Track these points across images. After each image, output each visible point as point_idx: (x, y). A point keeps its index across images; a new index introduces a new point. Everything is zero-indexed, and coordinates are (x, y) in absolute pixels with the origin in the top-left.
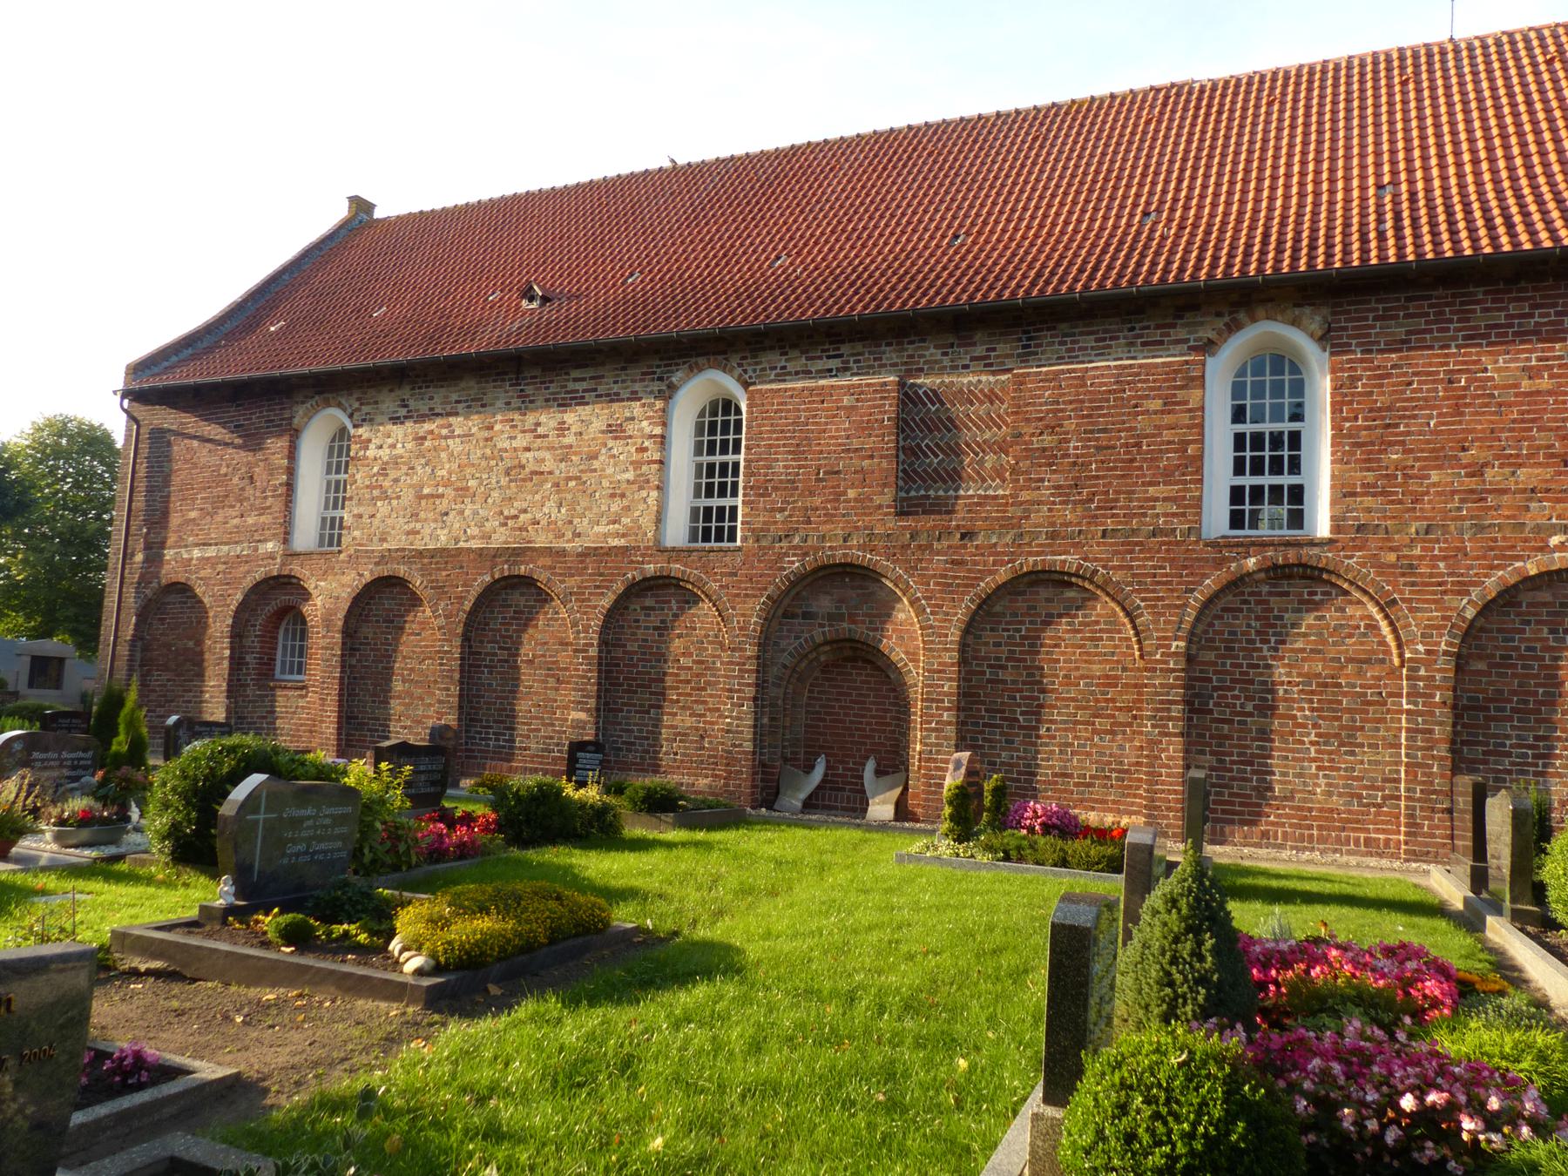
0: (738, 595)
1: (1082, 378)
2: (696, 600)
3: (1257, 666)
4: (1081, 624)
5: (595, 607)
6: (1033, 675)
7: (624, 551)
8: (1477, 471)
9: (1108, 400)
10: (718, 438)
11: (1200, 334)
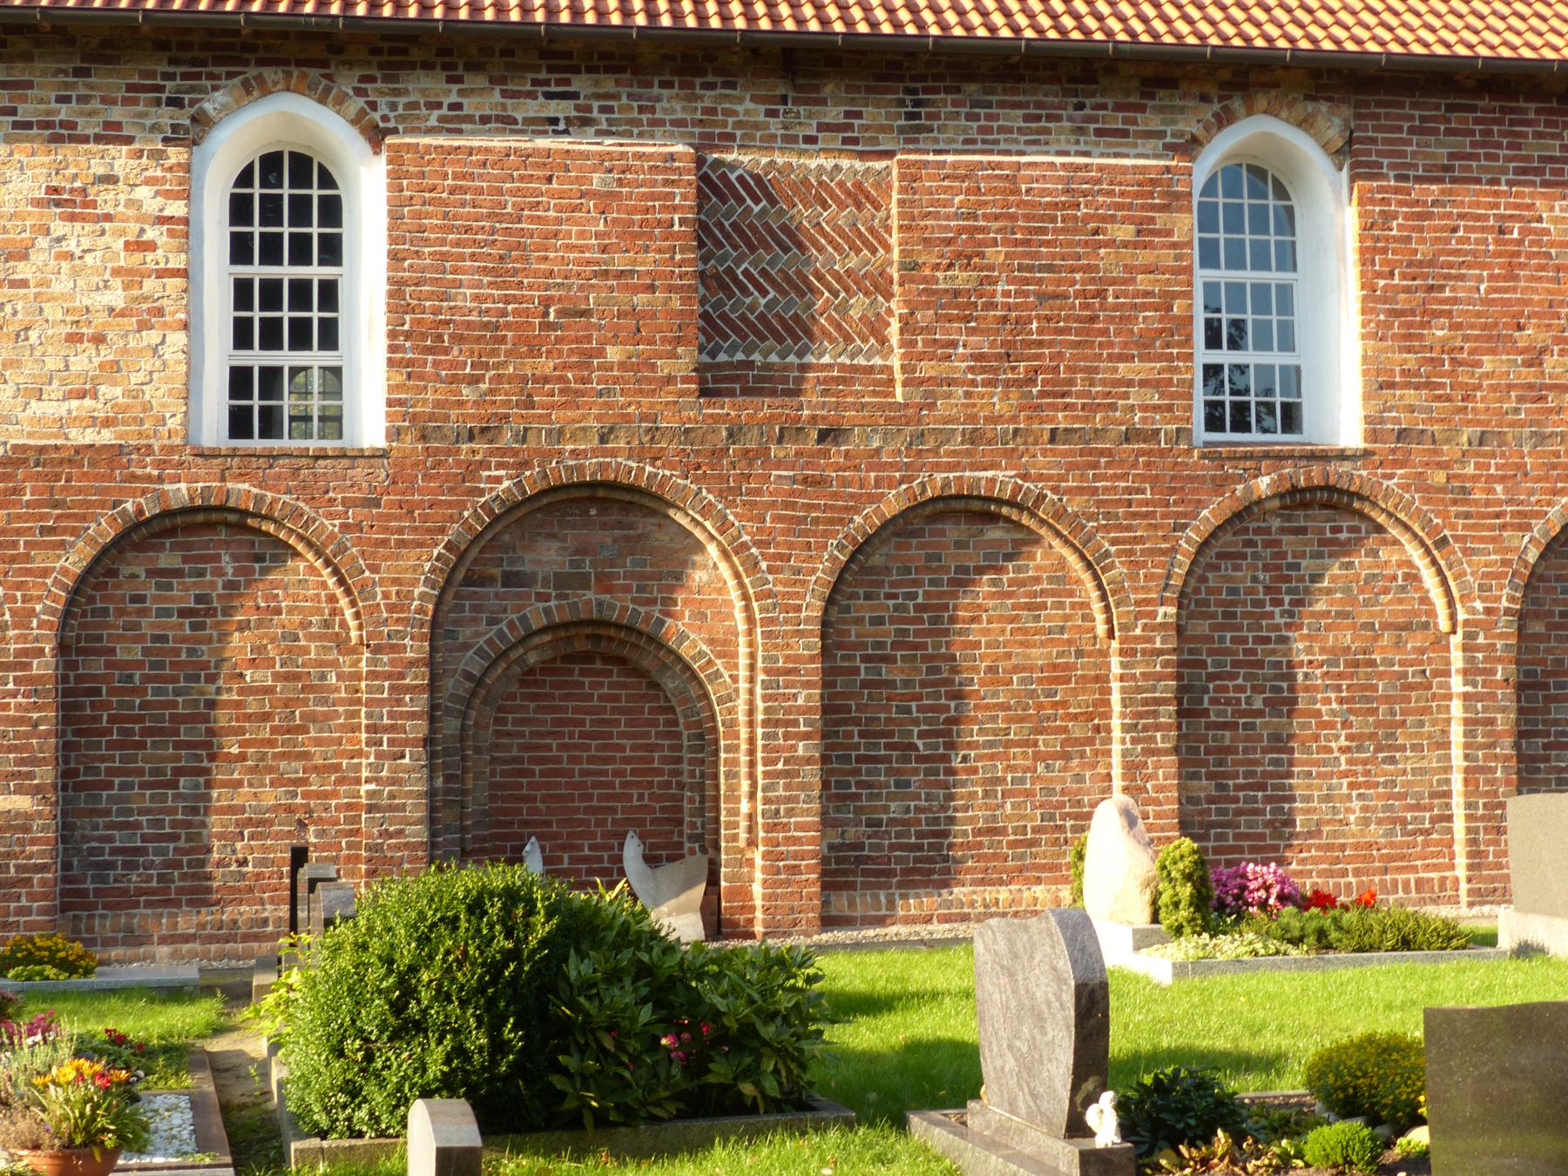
0: (384, 543)
1: (1012, 179)
2: (281, 552)
3: (1267, 640)
4: (1011, 583)
5: (45, 573)
6: (937, 670)
7: (114, 454)
8: (1535, 358)
10: (286, 230)
11: (1180, 127)
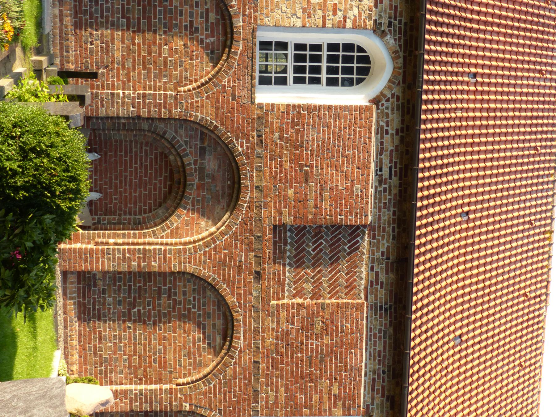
0: (218, 101)
2: (215, 61)
6: (165, 317)
9: (340, 362)
11: (375, 411)
